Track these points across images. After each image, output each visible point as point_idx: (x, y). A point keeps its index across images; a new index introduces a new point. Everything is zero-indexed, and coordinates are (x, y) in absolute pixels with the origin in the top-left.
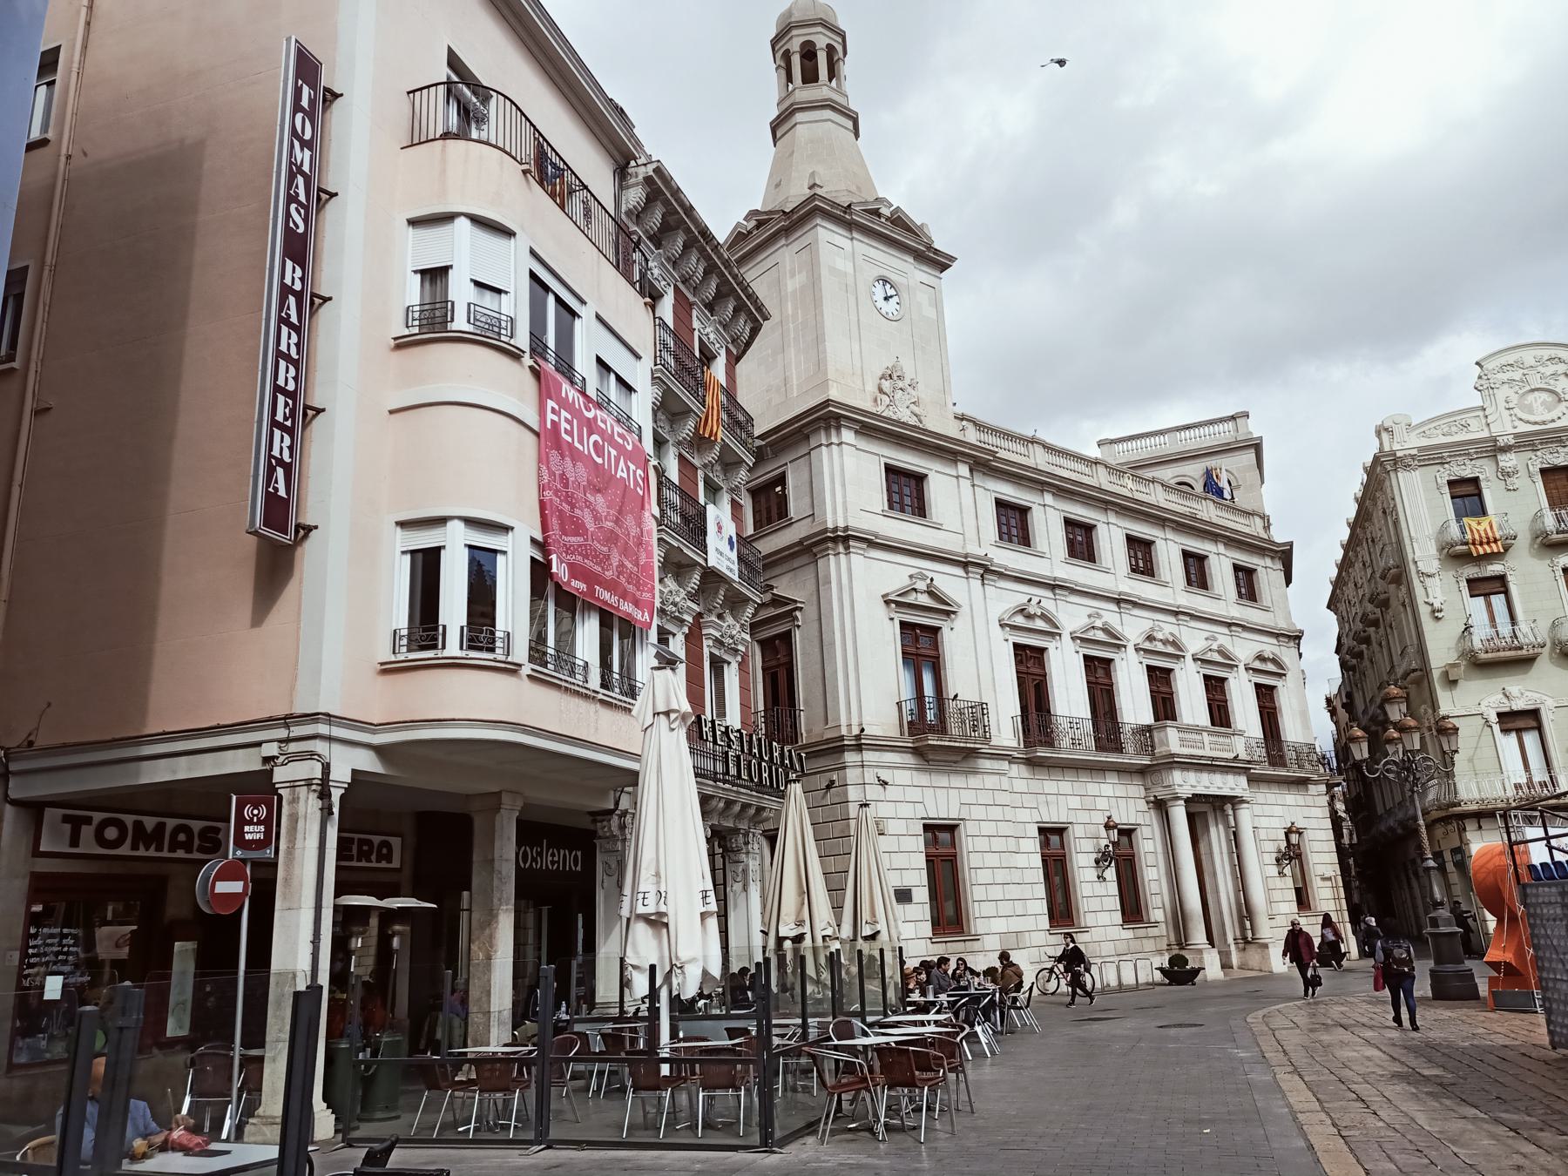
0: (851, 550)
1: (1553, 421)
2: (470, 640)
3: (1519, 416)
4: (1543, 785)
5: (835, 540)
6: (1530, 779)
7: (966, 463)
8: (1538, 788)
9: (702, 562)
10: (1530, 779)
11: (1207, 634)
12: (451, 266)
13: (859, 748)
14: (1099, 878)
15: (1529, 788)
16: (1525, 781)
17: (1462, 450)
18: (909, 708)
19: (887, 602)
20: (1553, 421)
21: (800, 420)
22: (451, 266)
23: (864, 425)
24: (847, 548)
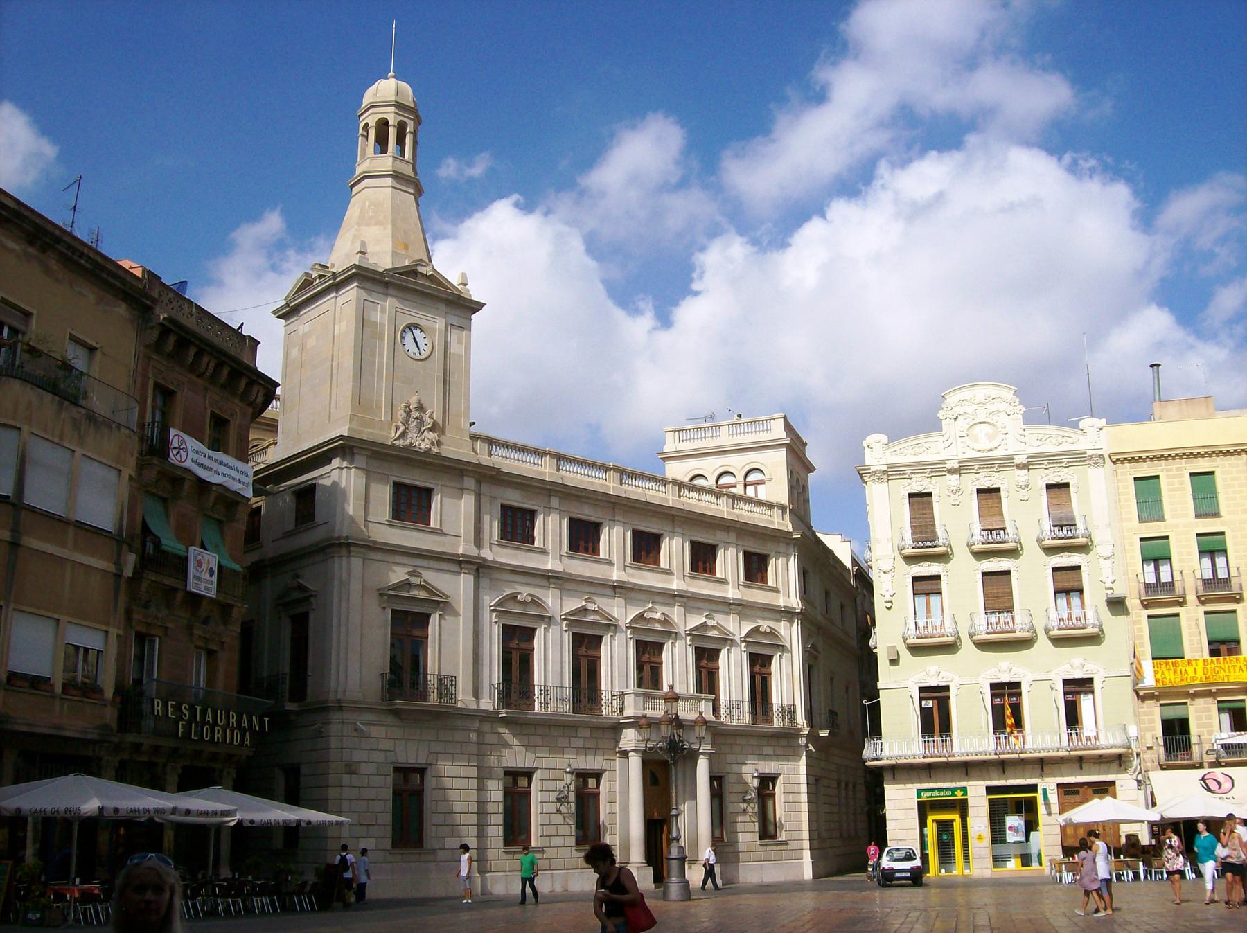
0: (352, 554)
1: (991, 450)
2: (1028, 859)
3: (972, 446)
4: (1078, 619)
5: (340, 545)
6: (1070, 614)
7: (472, 477)
8: (1075, 622)
9: (180, 586)
10: (1070, 614)
11: (410, 569)
12: (485, 304)
13: (341, 708)
14: (557, 811)
15: (1068, 620)
16: (1067, 616)
17: (985, 464)
18: (549, 696)
19: (381, 595)
20: (991, 450)
21: (319, 449)
22: (485, 304)
23: (374, 452)
24: (349, 552)
